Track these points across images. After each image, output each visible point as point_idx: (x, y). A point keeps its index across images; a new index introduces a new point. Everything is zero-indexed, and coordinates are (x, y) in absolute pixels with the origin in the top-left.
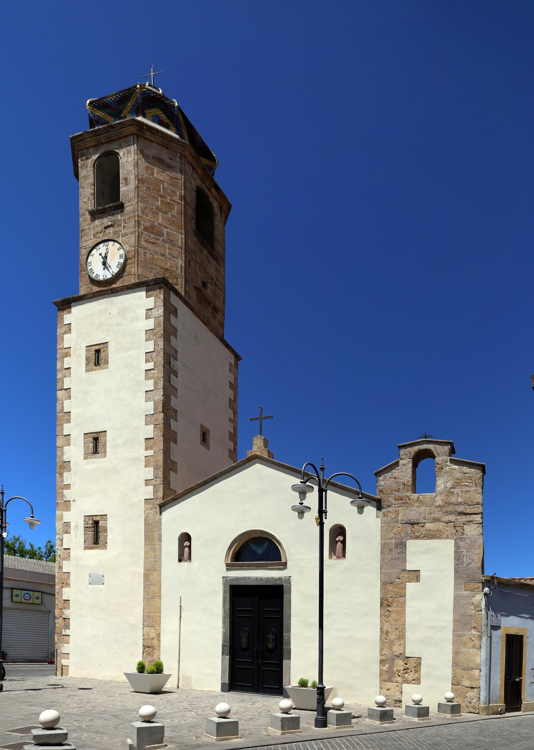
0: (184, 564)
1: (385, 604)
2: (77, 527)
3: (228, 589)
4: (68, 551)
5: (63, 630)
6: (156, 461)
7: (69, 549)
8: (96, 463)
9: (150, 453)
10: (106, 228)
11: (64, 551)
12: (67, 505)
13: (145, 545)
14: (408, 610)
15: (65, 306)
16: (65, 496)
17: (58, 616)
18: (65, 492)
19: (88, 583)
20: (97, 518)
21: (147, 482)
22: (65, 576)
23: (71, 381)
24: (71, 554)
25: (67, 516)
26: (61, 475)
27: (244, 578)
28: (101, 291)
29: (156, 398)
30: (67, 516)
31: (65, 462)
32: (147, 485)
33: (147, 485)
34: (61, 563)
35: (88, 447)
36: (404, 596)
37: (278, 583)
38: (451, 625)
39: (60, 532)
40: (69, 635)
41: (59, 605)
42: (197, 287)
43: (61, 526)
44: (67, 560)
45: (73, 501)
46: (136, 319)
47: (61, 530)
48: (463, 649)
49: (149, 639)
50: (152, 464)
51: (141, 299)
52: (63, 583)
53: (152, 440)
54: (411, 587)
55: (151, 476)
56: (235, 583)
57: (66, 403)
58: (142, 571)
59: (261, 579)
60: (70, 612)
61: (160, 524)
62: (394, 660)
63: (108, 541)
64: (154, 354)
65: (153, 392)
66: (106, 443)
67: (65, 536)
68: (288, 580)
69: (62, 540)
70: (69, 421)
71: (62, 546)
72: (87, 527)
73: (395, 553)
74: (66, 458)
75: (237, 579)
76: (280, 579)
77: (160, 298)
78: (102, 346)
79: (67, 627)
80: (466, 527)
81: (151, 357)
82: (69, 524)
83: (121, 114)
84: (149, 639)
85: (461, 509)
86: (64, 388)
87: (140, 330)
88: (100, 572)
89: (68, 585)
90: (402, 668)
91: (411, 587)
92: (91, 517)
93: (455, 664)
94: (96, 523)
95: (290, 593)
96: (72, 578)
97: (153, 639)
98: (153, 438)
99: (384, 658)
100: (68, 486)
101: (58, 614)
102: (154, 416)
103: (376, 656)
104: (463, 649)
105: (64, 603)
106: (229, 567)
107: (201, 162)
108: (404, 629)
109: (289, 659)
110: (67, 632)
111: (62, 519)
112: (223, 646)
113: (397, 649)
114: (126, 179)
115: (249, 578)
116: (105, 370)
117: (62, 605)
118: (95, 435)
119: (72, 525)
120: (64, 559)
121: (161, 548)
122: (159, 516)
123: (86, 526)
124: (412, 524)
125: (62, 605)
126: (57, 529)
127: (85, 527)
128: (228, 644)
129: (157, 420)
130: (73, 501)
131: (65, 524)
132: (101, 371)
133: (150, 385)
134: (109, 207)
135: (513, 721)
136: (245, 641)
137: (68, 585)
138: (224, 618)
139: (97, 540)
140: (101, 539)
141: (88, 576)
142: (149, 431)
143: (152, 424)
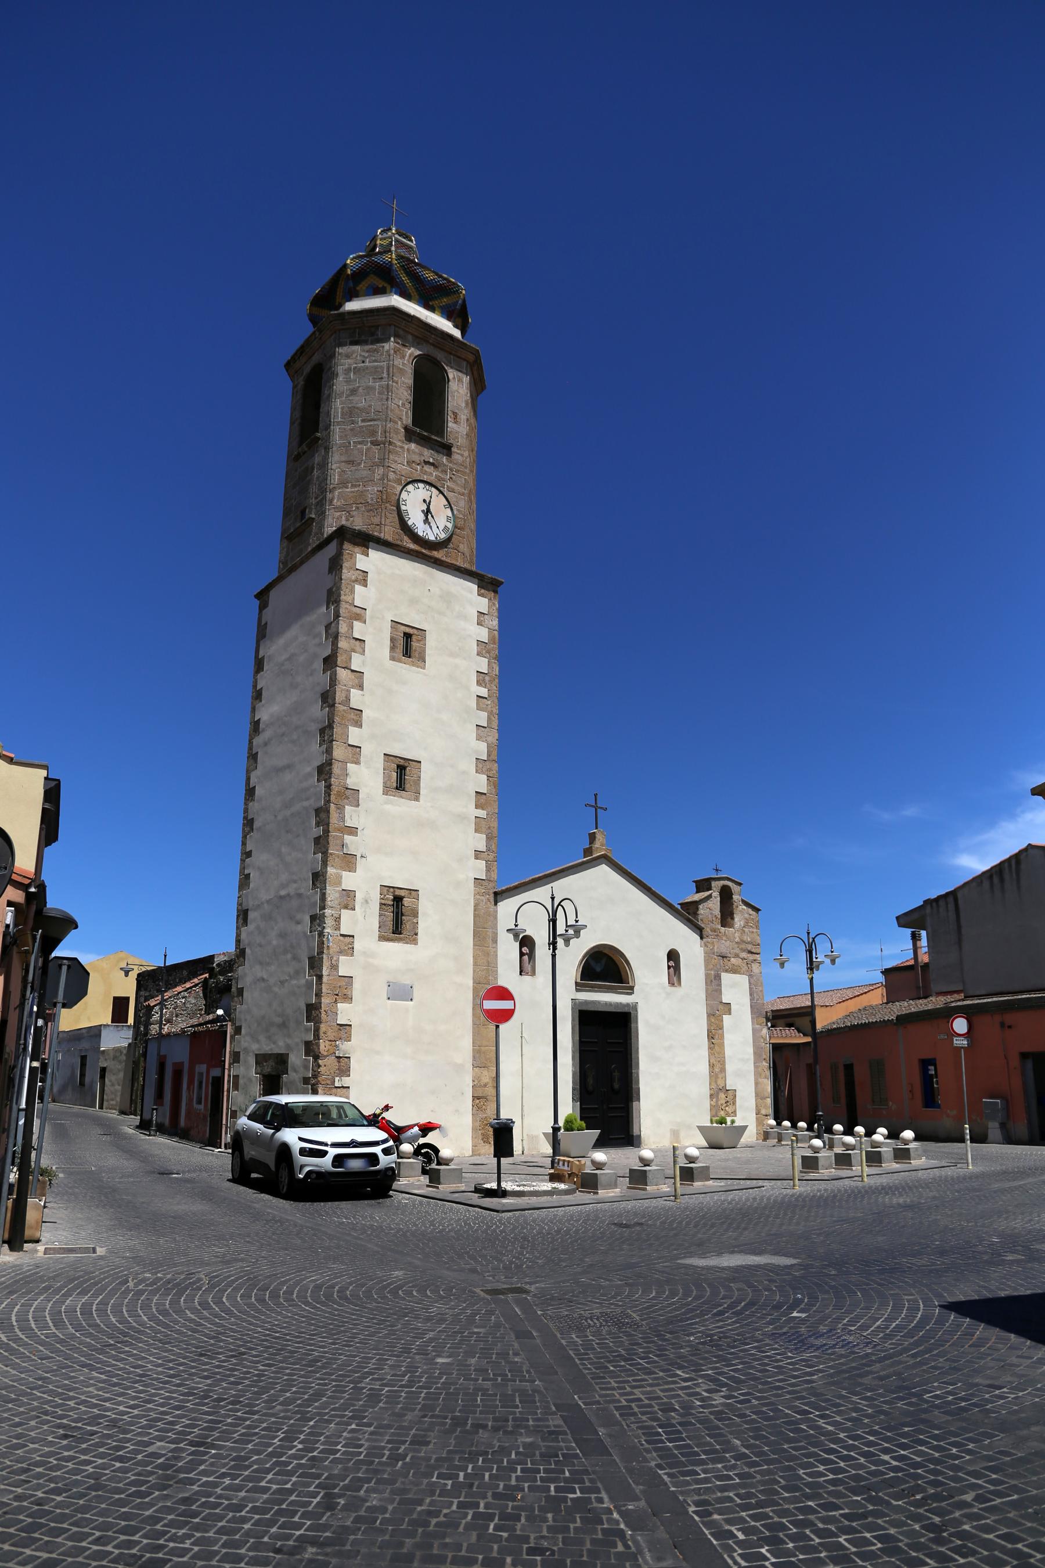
0: (527, 978)
1: (711, 1036)
2: (367, 902)
3: (577, 1015)
4: (348, 940)
5: (337, 1079)
6: (489, 828)
7: (353, 936)
8: (399, 806)
9: (482, 813)
10: (427, 463)
11: (342, 938)
12: (350, 862)
13: (474, 945)
14: (726, 1042)
15: (357, 540)
16: (347, 847)
17: (326, 1054)
18: (348, 838)
19: (386, 997)
20: (402, 893)
21: (478, 854)
22: (343, 983)
23: (363, 663)
24: (356, 946)
25: (349, 880)
26: (341, 809)
27: (594, 1002)
28: (417, 551)
29: (490, 739)
30: (349, 880)
31: (347, 788)
32: (476, 858)
33: (476, 858)
34: (335, 958)
35: (390, 777)
36: (722, 1028)
37: (626, 1010)
38: (752, 1057)
39: (335, 903)
40: (349, 1087)
41: (329, 1034)
42: (317, 442)
43: (337, 895)
44: (347, 955)
45: (362, 857)
46: (462, 617)
47: (336, 902)
48: (760, 1080)
49: (480, 1086)
50: (484, 830)
51: (471, 592)
52: (337, 995)
53: (484, 796)
54: (726, 1018)
55: (482, 846)
56: (584, 1008)
57: (354, 693)
58: (471, 983)
59: (610, 1004)
60: (354, 1048)
61: (496, 918)
62: (718, 1093)
63: (420, 931)
64: (487, 678)
65: (486, 730)
66: (419, 780)
67: (345, 914)
68: (635, 1007)
69: (338, 920)
70: (359, 724)
71: (338, 928)
72: (384, 904)
73: (715, 982)
74: (350, 782)
75: (586, 1002)
76: (628, 1005)
77: (494, 604)
78: (415, 631)
79: (345, 1071)
80: (753, 965)
81: (484, 680)
82: (352, 894)
83: (431, 300)
84: (480, 1086)
85: (750, 947)
86: (352, 668)
87: (470, 636)
88: (406, 980)
89: (348, 998)
90: (724, 1102)
91: (726, 1018)
92: (392, 890)
93: (757, 1095)
94: (398, 900)
95: (637, 1022)
96: (357, 985)
97: (485, 1086)
98: (485, 794)
99: (712, 1092)
100: (353, 831)
101: (326, 1049)
102: (487, 763)
103: (706, 1091)
104: (760, 1080)
105: (340, 1030)
106: (579, 988)
107: (412, 334)
108: (724, 1062)
109: (639, 1100)
110: (346, 1081)
111: (340, 883)
112: (574, 1089)
113: (721, 1083)
114: (455, 414)
115: (599, 1002)
116: (419, 669)
117: (334, 1034)
118: (402, 762)
119: (359, 896)
120: (341, 952)
121: (496, 952)
122: (493, 907)
123: (383, 902)
124: (723, 957)
125: (334, 1034)
126: (329, 899)
127: (381, 904)
128: (578, 1087)
129: (490, 770)
130: (362, 857)
131: (344, 892)
132: (414, 668)
133: (482, 718)
134: (436, 441)
135: (336, 1095)
136: (592, 1082)
137: (348, 998)
138: (573, 1052)
139: (397, 927)
140: (407, 926)
141: (386, 987)
142: (481, 782)
143: (484, 774)
